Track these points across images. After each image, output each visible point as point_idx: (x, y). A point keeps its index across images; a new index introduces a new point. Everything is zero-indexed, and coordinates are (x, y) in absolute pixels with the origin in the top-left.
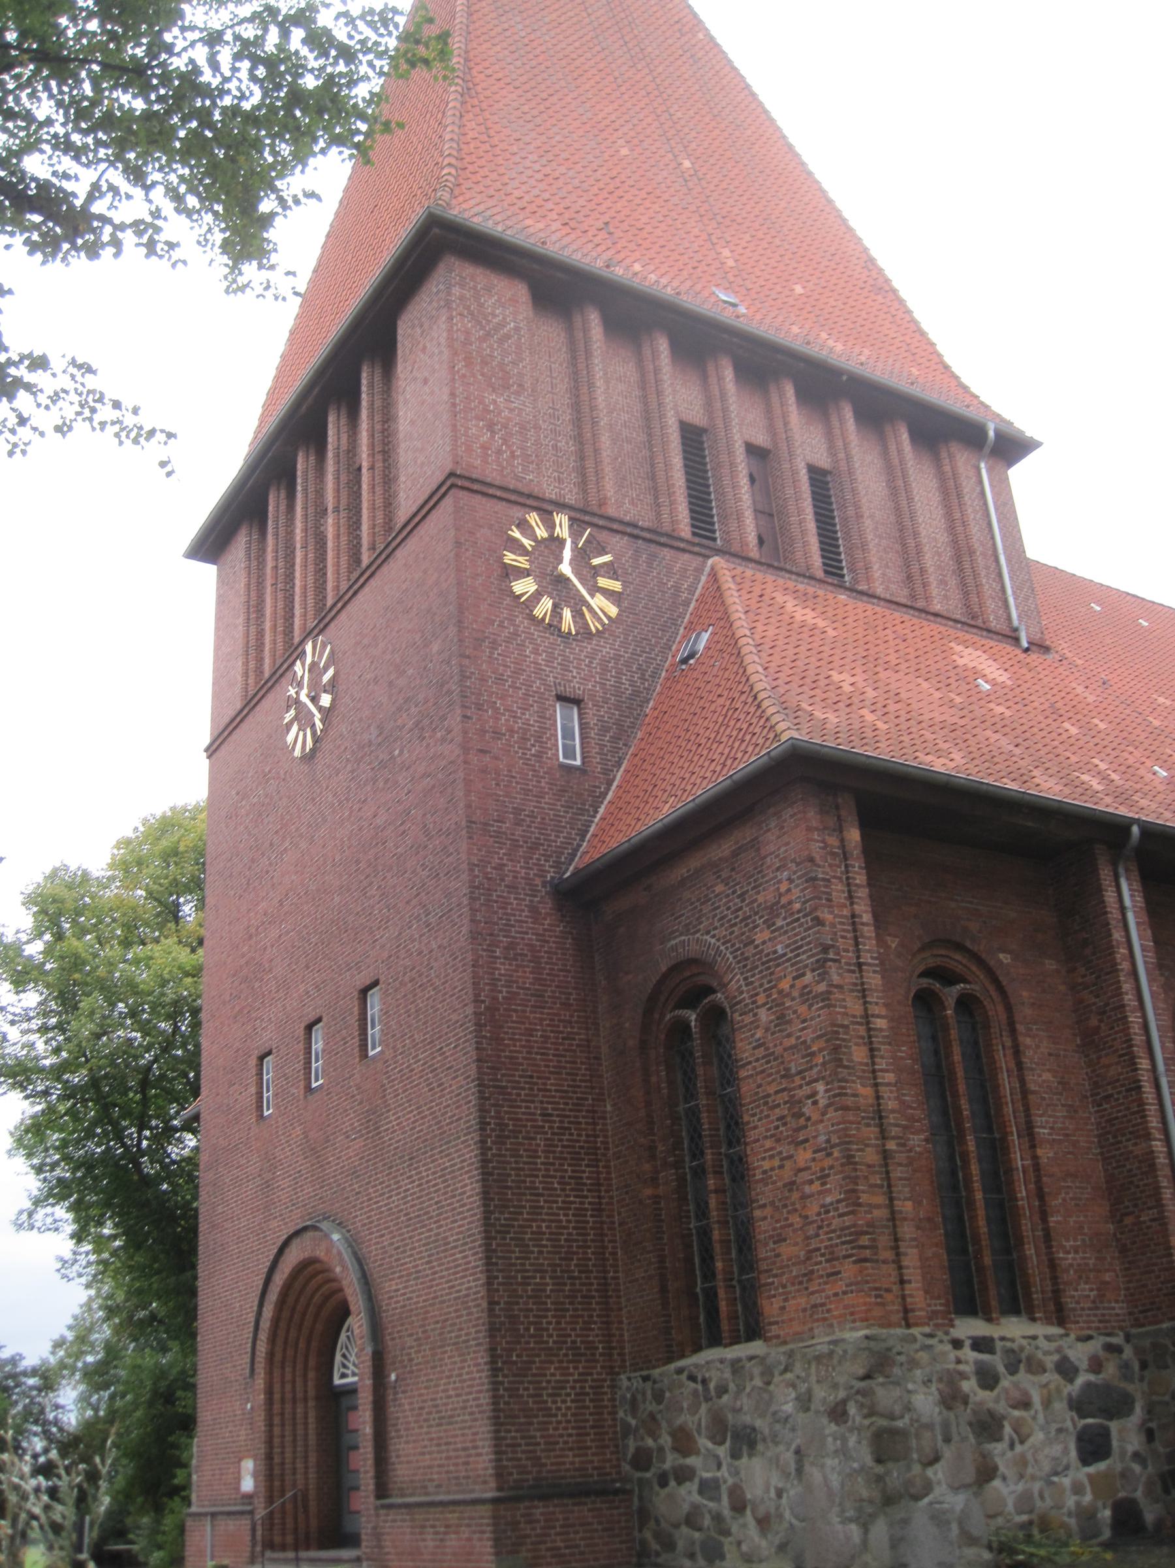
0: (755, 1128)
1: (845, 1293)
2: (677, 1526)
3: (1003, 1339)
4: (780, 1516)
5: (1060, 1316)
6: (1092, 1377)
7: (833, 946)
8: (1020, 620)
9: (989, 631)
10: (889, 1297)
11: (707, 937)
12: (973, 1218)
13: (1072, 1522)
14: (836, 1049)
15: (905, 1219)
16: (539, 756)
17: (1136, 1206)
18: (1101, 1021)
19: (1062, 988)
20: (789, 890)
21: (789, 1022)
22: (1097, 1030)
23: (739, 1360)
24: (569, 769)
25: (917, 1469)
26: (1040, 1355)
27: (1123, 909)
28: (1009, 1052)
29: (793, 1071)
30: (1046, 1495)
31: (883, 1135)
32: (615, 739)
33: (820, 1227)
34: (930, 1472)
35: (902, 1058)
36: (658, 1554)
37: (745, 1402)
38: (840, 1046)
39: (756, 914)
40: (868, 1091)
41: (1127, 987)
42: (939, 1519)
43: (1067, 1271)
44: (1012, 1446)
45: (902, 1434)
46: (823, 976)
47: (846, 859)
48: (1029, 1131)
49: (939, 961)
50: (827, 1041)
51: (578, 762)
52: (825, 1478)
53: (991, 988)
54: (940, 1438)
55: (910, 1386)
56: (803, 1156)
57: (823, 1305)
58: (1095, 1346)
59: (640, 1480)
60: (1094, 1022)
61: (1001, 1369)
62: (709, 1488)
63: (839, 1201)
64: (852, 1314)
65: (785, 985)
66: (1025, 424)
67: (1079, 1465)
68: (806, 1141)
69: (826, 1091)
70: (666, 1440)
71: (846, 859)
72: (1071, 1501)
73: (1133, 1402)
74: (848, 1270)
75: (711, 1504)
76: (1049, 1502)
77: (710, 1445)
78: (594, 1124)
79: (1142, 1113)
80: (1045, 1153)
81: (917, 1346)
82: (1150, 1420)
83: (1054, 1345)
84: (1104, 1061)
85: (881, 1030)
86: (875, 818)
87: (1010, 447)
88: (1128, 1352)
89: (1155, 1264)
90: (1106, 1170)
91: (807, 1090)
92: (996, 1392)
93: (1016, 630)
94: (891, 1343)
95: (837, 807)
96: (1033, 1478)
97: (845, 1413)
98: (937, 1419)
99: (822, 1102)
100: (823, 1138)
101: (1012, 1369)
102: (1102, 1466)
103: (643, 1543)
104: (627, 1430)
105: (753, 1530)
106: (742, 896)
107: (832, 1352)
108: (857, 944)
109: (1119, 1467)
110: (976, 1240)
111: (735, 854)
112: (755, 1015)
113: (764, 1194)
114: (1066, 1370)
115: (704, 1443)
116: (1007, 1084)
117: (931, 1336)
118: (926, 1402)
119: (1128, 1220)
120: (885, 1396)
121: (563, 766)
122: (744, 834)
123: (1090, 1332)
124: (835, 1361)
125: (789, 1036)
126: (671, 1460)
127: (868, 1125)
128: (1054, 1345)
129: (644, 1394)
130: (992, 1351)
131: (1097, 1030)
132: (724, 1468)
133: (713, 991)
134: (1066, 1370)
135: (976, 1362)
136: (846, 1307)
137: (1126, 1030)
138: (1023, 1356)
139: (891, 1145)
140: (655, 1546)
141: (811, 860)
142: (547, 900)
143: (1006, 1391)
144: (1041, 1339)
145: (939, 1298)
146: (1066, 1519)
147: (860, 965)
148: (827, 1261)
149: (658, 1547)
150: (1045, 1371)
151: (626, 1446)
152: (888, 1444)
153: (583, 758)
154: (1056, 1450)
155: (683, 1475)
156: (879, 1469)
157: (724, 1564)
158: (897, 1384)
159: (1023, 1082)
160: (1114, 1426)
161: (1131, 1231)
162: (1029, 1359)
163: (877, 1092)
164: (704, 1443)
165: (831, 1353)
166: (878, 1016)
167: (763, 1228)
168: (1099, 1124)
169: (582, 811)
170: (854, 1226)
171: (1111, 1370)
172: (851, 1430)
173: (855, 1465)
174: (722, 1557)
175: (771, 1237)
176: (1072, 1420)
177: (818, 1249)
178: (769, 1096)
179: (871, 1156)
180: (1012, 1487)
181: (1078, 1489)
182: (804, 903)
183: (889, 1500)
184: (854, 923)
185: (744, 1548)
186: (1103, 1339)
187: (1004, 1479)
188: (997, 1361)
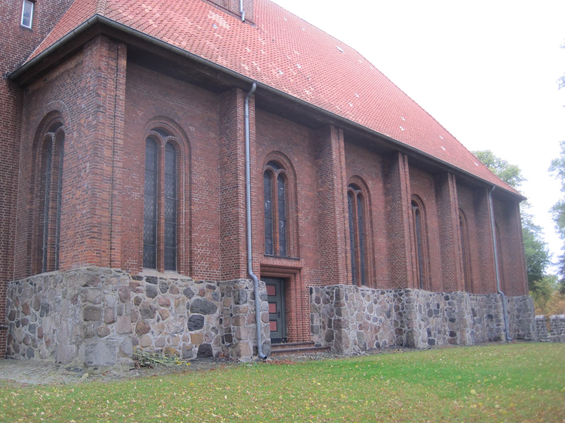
0: (66, 181)
1: (85, 251)
2: (20, 343)
3: (161, 278)
4: (53, 341)
5: (191, 273)
6: (200, 298)
7: (103, 106)
8: (244, 9)
9: (229, 11)
10: (103, 254)
11: (61, 101)
12: (159, 230)
14: (96, 149)
15: (117, 223)
16: (10, 20)
17: (229, 233)
18: (228, 159)
19: (216, 145)
20: (90, 81)
21: (81, 137)
22: (226, 163)
23: (47, 277)
24: (24, 29)
25: (103, 325)
26: (177, 286)
27: (244, 116)
28: (187, 167)
29: (80, 157)
30: (171, 341)
31: (113, 188)
32: (49, 20)
33: (80, 223)
34: (109, 326)
35: (135, 160)
36: (13, 354)
37: (47, 294)
38: (98, 148)
39: (79, 92)
40: (109, 169)
41: (240, 147)
42: (110, 346)
43: (197, 256)
44: (158, 320)
45: (99, 310)
46: (96, 117)
47: (117, 71)
48: (190, 199)
49: (162, 125)
50: (93, 145)
51: (30, 27)
52: (67, 326)
53: (184, 140)
54: (116, 313)
55: (106, 291)
56: (79, 193)
57: (77, 255)
58: (203, 286)
59: (11, 324)
60: (226, 160)
61: (158, 290)
62: (32, 328)
63: (88, 213)
64: (86, 259)
65: (82, 121)
67: (188, 330)
68: (80, 187)
69: (90, 166)
70: (21, 308)
71: (117, 71)
72: (181, 344)
73: (216, 309)
74: (87, 241)
75: (32, 335)
76: (171, 343)
77: (34, 311)
78: (12, 178)
79: (237, 197)
80: (195, 209)
81: (112, 275)
82: (222, 316)
83: (184, 284)
84: (227, 175)
85: (120, 144)
88: (218, 289)
89: (233, 257)
90: (221, 219)
91: (83, 166)
92: (154, 299)
93: (241, 13)
94: (98, 273)
95: (118, 50)
96: (166, 334)
97: (77, 300)
98: (116, 306)
99: (88, 171)
100: (86, 186)
101: (164, 291)
102: (198, 331)
103: (8, 349)
104: (9, 304)
105: (44, 346)
106: (75, 84)
107: (76, 274)
108: (115, 107)
109: (205, 332)
110: (159, 239)
111: (76, 66)
112: (72, 134)
113: (65, 209)
114: (188, 293)
115: (32, 310)
116: (184, 179)
117: (120, 272)
118: (112, 298)
119: (226, 239)
120: (92, 294)
121: (21, 27)
122: (78, 59)
123: (202, 280)
124: (76, 278)
125: (81, 143)
126: (21, 317)
127: (106, 183)
128: (184, 284)
129: (16, 289)
130: (155, 283)
131: (226, 163)
132: (38, 320)
133: (62, 125)
134: (188, 293)
136: (84, 257)
137: (236, 164)
138: (169, 286)
139: (116, 192)
140: (13, 351)
141: (100, 69)
142: (4, 81)
143: (159, 299)
144: (179, 280)
145: (136, 259)
146: (178, 350)
147: (115, 116)
148: (81, 237)
149: (14, 351)
150: (179, 293)
151: (8, 310)
152: (91, 314)
153: (33, 25)
154: (179, 323)
155: (24, 322)
156: (85, 323)
157: (34, 359)
158: (100, 290)
159: (191, 179)
160: (206, 317)
161: (227, 243)
163: (113, 169)
164: (32, 310)
166: (120, 139)
167: (63, 223)
168: (221, 200)
169: (27, 47)
170: (91, 223)
171: (209, 295)
172: (78, 307)
173: (77, 321)
174: (33, 356)
175: (65, 227)
176: (188, 312)
177: (78, 232)
178: (72, 168)
179: (106, 196)
180: (156, 336)
181: (185, 339)
182: (94, 87)
183: (87, 336)
184: (116, 99)
185: (41, 353)
187: (153, 333)
188: (157, 287)
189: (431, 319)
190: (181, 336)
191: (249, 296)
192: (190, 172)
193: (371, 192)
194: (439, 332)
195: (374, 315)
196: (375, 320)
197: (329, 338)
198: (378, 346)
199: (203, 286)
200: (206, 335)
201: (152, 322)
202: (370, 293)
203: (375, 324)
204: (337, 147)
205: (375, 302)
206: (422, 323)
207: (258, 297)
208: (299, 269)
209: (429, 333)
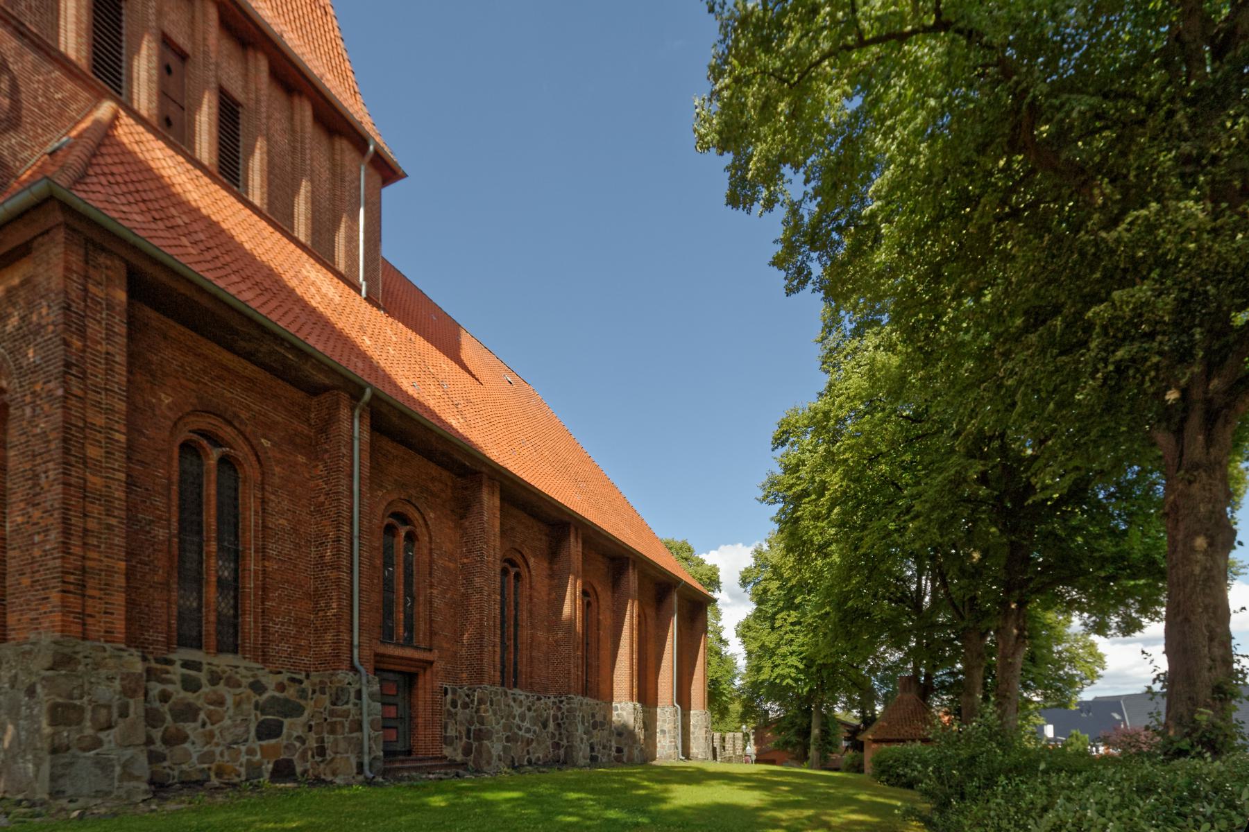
5: (265, 659)
6: (277, 694)
13: (243, 770)
34: (102, 735)
42: (103, 766)
44: (204, 725)
58: (283, 678)
60: (322, 499)
61: (204, 681)
66: (397, 155)
72: (244, 759)
85: (118, 441)
86: (139, 287)
87: (386, 171)
102: (273, 741)
109: (285, 743)
118: (108, 692)
119: (321, 614)
130: (199, 670)
134: (258, 687)
135: (183, 675)
138: (225, 676)
152: (62, 714)
160: (287, 722)
162: (229, 678)
165: (30, 652)
186: (289, 675)
187: (193, 743)
188: (203, 677)
189: (595, 732)
190: (243, 748)
191: (353, 695)
192: (264, 510)
193: (533, 573)
194: (604, 748)
195: (526, 724)
196: (528, 730)
197: (467, 751)
198: (530, 762)
199: (283, 678)
200: (286, 747)
201: (189, 728)
202: (522, 698)
203: (528, 735)
204: (490, 502)
205: (529, 709)
206: (585, 737)
207: (365, 696)
208: (431, 663)
209: (592, 749)
